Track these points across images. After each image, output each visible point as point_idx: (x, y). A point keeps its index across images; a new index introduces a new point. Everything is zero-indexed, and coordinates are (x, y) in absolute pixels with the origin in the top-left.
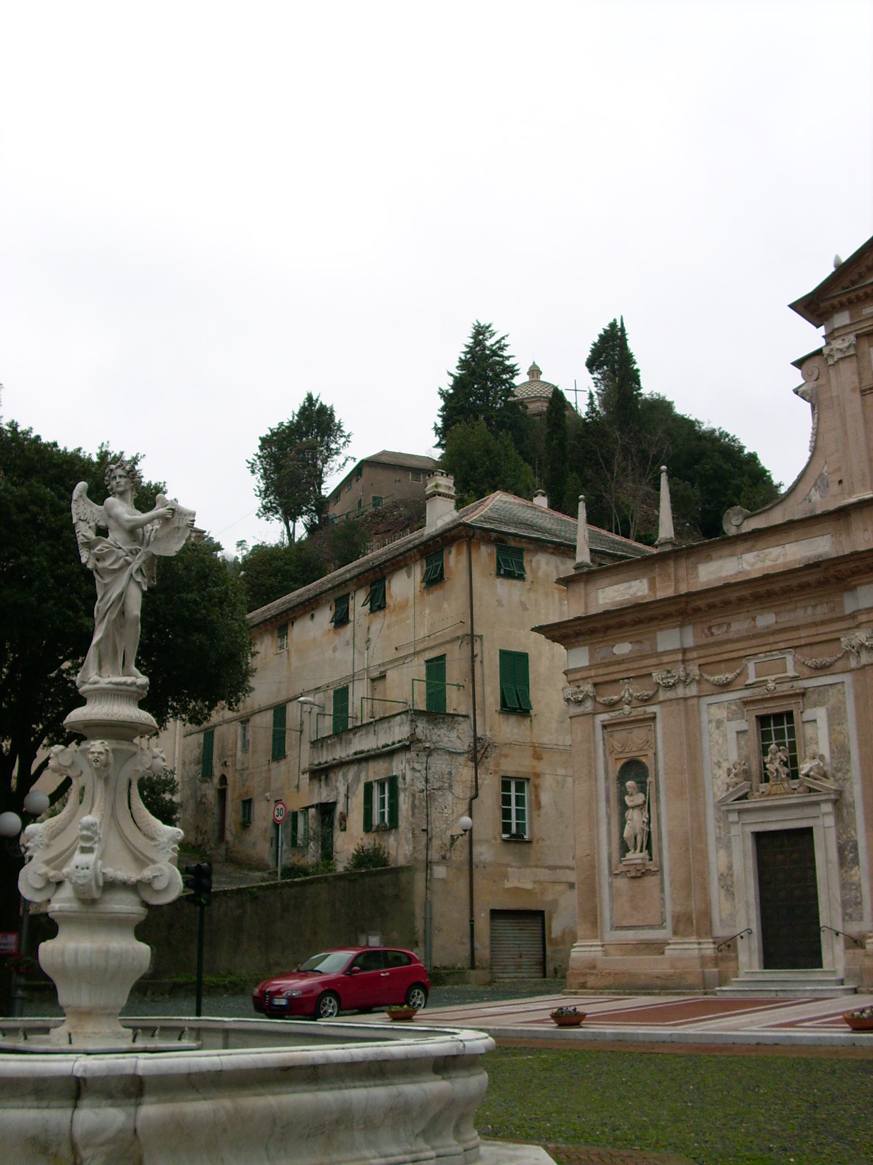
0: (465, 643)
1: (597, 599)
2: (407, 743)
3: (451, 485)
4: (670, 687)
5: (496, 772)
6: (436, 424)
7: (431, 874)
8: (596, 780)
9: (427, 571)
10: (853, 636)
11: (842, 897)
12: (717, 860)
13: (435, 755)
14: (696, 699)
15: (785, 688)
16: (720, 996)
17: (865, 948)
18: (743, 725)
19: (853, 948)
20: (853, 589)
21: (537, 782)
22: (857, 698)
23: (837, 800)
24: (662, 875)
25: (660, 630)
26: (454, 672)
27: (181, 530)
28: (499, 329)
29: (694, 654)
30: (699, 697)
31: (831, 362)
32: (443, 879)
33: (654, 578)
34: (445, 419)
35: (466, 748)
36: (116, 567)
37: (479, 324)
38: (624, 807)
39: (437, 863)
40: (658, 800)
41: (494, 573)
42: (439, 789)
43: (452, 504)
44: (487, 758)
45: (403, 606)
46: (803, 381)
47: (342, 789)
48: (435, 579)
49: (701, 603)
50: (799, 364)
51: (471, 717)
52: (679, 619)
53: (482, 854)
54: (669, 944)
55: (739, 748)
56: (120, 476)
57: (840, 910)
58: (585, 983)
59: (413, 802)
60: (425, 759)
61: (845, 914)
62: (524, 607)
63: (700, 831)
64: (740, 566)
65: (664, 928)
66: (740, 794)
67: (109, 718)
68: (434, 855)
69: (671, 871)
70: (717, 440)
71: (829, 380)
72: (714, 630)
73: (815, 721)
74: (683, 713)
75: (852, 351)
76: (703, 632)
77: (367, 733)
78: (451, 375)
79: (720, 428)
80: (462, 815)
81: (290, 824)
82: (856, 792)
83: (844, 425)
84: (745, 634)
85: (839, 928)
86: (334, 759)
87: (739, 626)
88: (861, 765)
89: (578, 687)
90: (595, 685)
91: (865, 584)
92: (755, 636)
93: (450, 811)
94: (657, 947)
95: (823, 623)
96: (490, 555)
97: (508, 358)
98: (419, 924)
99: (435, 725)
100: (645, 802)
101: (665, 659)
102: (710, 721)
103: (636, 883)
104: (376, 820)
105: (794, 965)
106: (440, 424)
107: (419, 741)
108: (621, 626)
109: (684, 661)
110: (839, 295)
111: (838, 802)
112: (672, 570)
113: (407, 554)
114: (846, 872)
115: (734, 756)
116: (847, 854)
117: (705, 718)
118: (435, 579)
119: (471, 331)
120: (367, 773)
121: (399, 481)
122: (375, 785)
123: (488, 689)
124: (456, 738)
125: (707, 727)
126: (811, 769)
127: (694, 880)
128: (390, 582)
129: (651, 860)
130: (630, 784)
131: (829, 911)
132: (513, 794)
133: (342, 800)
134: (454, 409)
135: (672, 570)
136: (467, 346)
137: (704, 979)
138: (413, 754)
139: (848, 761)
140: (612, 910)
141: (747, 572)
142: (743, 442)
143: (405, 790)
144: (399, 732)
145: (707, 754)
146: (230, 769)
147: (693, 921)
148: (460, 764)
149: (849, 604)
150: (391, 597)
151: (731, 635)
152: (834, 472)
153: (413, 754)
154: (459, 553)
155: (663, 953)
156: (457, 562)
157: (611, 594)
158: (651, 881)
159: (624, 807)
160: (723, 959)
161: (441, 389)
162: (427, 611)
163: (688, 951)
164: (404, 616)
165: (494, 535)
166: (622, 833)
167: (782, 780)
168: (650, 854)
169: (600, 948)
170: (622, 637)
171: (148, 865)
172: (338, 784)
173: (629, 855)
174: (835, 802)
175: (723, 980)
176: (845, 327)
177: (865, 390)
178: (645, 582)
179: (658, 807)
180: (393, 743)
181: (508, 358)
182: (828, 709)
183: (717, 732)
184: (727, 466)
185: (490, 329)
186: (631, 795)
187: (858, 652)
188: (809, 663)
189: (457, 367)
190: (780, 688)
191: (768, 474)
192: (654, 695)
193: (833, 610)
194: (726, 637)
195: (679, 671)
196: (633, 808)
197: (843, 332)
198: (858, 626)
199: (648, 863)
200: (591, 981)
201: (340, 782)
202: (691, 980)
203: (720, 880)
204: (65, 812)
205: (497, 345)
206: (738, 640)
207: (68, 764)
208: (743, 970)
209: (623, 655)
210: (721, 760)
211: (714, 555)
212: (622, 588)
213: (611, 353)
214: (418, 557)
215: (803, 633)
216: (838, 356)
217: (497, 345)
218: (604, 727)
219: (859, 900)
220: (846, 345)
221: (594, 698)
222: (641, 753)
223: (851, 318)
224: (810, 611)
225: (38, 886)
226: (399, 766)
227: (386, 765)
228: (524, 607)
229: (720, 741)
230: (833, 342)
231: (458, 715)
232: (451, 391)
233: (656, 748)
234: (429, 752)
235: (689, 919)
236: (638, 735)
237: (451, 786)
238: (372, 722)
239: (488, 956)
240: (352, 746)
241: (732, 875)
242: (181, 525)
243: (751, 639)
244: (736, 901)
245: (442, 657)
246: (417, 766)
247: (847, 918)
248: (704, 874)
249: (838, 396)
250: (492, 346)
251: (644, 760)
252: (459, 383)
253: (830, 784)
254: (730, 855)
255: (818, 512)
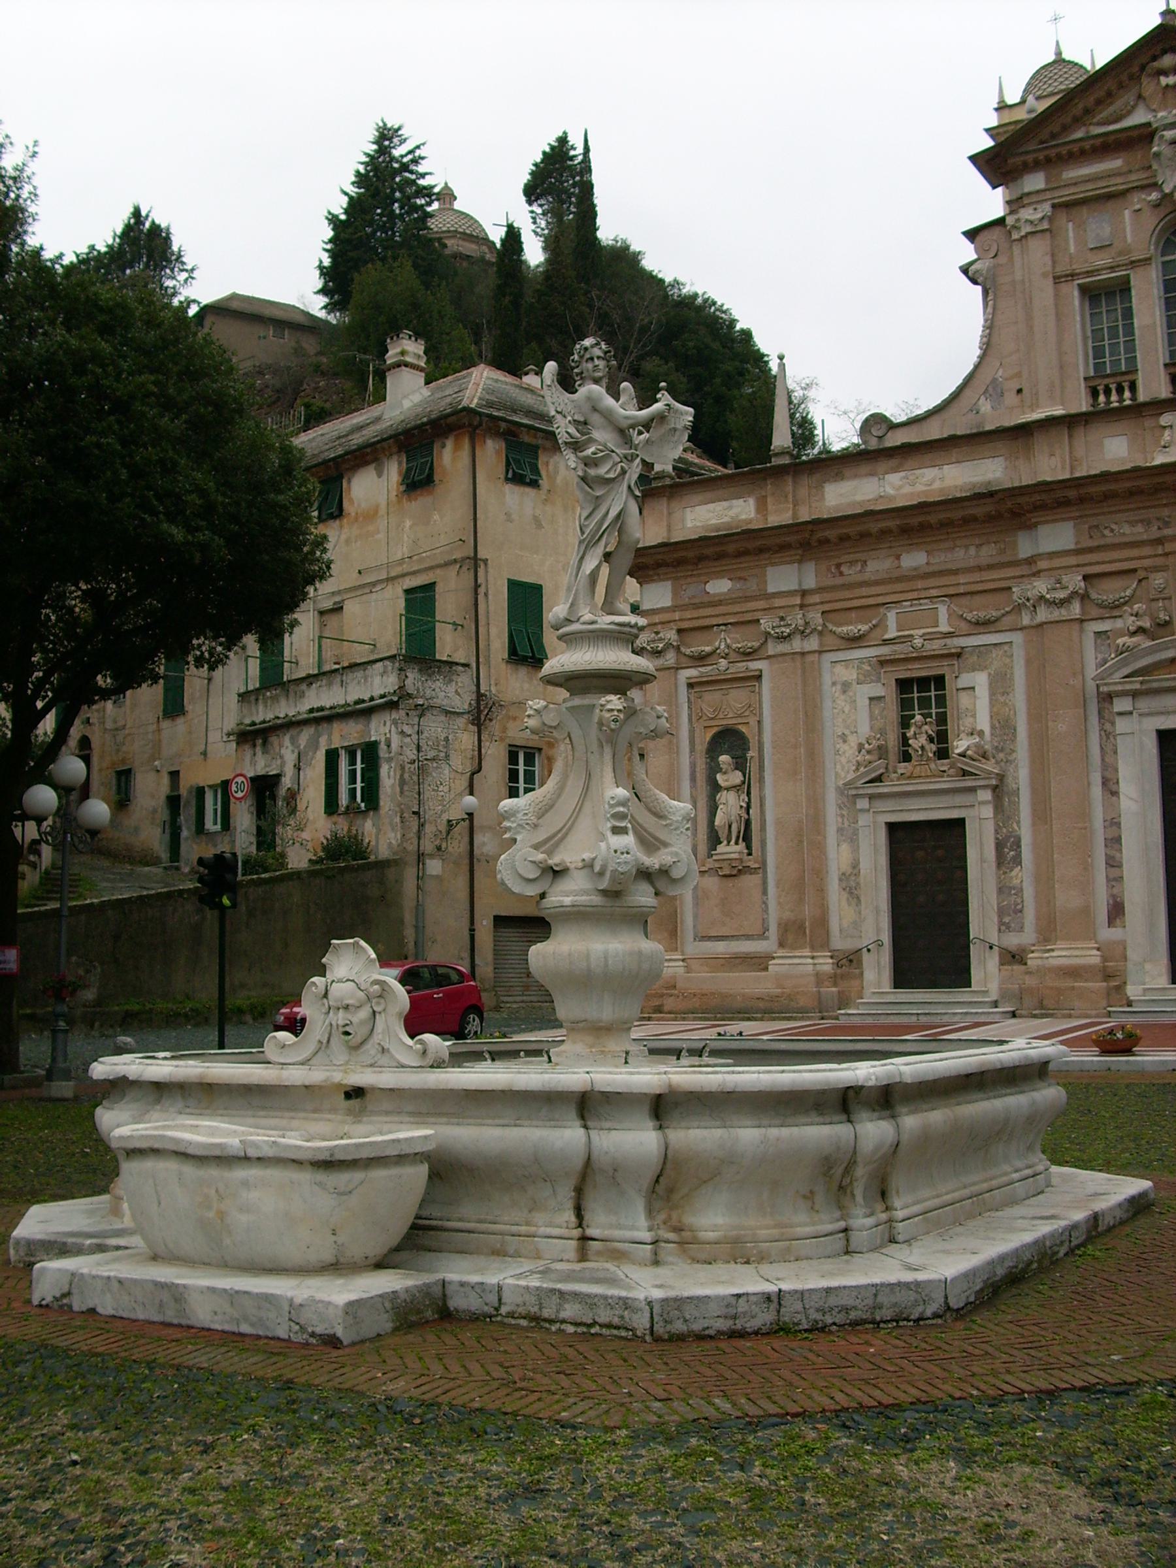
0: (465, 568)
1: (683, 520)
2: (395, 699)
3: (421, 353)
4: (785, 638)
5: (502, 739)
6: (321, 262)
7: (423, 869)
8: (678, 753)
9: (409, 470)
10: (1029, 587)
11: (998, 904)
12: (838, 856)
13: (428, 714)
14: (817, 655)
15: (935, 646)
16: (843, 1021)
17: (1026, 964)
18: (878, 690)
19: (1009, 963)
20: (1032, 527)
21: (550, 753)
22: (1028, 662)
23: (997, 787)
24: (765, 872)
25: (773, 564)
26: (449, 605)
27: (678, 433)
28: (413, 134)
29: (816, 598)
30: (820, 652)
31: (1015, 236)
32: (437, 876)
33: (765, 497)
34: (333, 254)
35: (466, 707)
36: (612, 475)
37: (385, 125)
38: (715, 788)
39: (431, 856)
40: (761, 780)
41: (502, 477)
42: (433, 759)
43: (420, 378)
44: (491, 720)
45: (371, 515)
46: (975, 257)
47: (290, 757)
48: (419, 481)
49: (831, 534)
50: (972, 235)
51: (476, 665)
52: (800, 552)
53: (484, 844)
54: (774, 958)
55: (872, 717)
56: (598, 358)
57: (996, 919)
58: (662, 1005)
59: (402, 776)
60: (417, 719)
61: (1001, 923)
62: (538, 523)
63: (817, 821)
64: (882, 489)
65: (767, 938)
66: (873, 775)
67: (622, 667)
68: (428, 846)
69: (777, 868)
70: (701, 309)
71: (1011, 258)
72: (844, 569)
73: (973, 688)
74: (799, 671)
75: (1045, 225)
76: (829, 570)
77: (330, 684)
78: (346, 194)
79: (705, 293)
80: (461, 795)
81: (194, 802)
82: (1021, 777)
83: (1029, 318)
84: (886, 576)
85: (994, 938)
86: (278, 718)
87: (878, 565)
88: (1030, 745)
89: (657, 633)
90: (680, 631)
91: (1047, 522)
92: (899, 579)
93: (446, 789)
94: (760, 962)
95: (990, 567)
96: (498, 452)
97: (423, 176)
98: (409, 933)
99: (430, 676)
100: (744, 782)
101: (778, 602)
102: (834, 684)
103: (730, 883)
104: (344, 799)
105: (933, 984)
106: (327, 262)
107: (410, 696)
108: (720, 557)
109: (802, 606)
110: (1035, 151)
111: (998, 790)
112: (790, 488)
113: (378, 446)
114: (1005, 873)
115: (864, 729)
116: (1006, 851)
117: (827, 679)
118: (419, 481)
119: (372, 134)
120: (330, 735)
121: (265, 338)
122: (342, 753)
123: (493, 631)
124: (454, 693)
125: (830, 691)
126: (968, 749)
127: (808, 878)
128: (349, 482)
129: (750, 854)
130: (724, 759)
131: (982, 919)
132: (521, 767)
133: (289, 771)
134: (349, 241)
135: (790, 488)
136: (368, 155)
137: (820, 1002)
138: (402, 713)
139: (1013, 740)
140: (696, 916)
141: (891, 498)
142: (736, 314)
143: (390, 760)
144: (380, 683)
145: (828, 724)
146: (96, 728)
147: (804, 931)
148: (459, 728)
149: (1025, 546)
150: (351, 501)
151: (867, 576)
152: (1011, 378)
153: (402, 713)
154: (457, 448)
155: (766, 969)
156: (454, 459)
157: (702, 516)
158: (750, 882)
159: (715, 788)
160: (843, 977)
161: (329, 213)
162: (408, 523)
163: (800, 967)
164: (371, 528)
165: (503, 425)
166: (711, 822)
167: (929, 759)
168: (749, 847)
169: (681, 963)
170: (718, 572)
171: (659, 849)
172: (283, 751)
173: (721, 848)
174: (995, 789)
175: (844, 1001)
176: (1038, 192)
177: (1059, 277)
178: (751, 502)
179: (761, 789)
180: (372, 699)
181: (423, 176)
182: (990, 674)
183: (843, 697)
184: (716, 345)
185: (400, 133)
186: (725, 773)
187: (1034, 607)
188: (969, 616)
189: (353, 183)
190: (928, 646)
191: (766, 359)
192: (759, 648)
193: (1002, 552)
194: (859, 578)
195: (796, 618)
196: (728, 789)
197: (1034, 198)
198: (1037, 574)
199: (746, 857)
200: (669, 1003)
201: (287, 749)
202: (802, 1002)
203: (840, 880)
204: (551, 784)
205: (410, 157)
206: (877, 583)
207: (554, 724)
208: (869, 990)
209: (718, 595)
210: (847, 732)
211: (847, 472)
212: (718, 508)
213: (561, 180)
214: (394, 450)
215: (962, 579)
216: (1029, 229)
217: (410, 157)
218: (690, 686)
219: (1019, 907)
220: (1039, 216)
221: (678, 648)
222: (740, 720)
223: (1047, 181)
224: (972, 551)
225: (531, 876)
226: (379, 729)
227: (360, 727)
228: (538, 523)
229: (847, 710)
230: (1022, 211)
231: (457, 664)
232: (343, 217)
233: (761, 714)
234: (422, 710)
235: (801, 928)
236: (737, 698)
237: (447, 756)
238: (336, 670)
239: (491, 975)
240: (305, 700)
241: (857, 875)
242: (678, 426)
243: (894, 583)
244: (863, 906)
245: (430, 587)
246: (407, 730)
247: (1003, 928)
248: (820, 874)
249: (1023, 281)
250: (402, 156)
251: (743, 729)
252: (355, 206)
253: (990, 766)
254: (855, 849)
255: (988, 427)
